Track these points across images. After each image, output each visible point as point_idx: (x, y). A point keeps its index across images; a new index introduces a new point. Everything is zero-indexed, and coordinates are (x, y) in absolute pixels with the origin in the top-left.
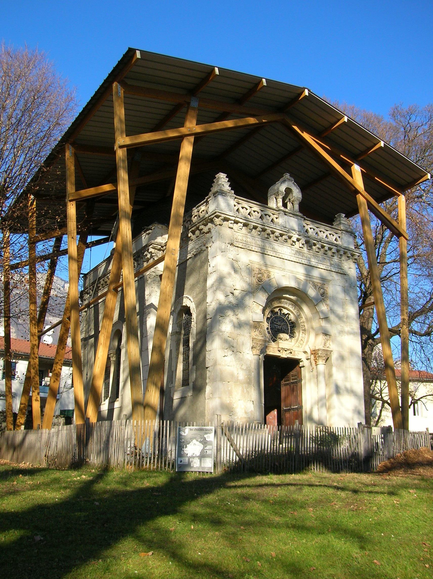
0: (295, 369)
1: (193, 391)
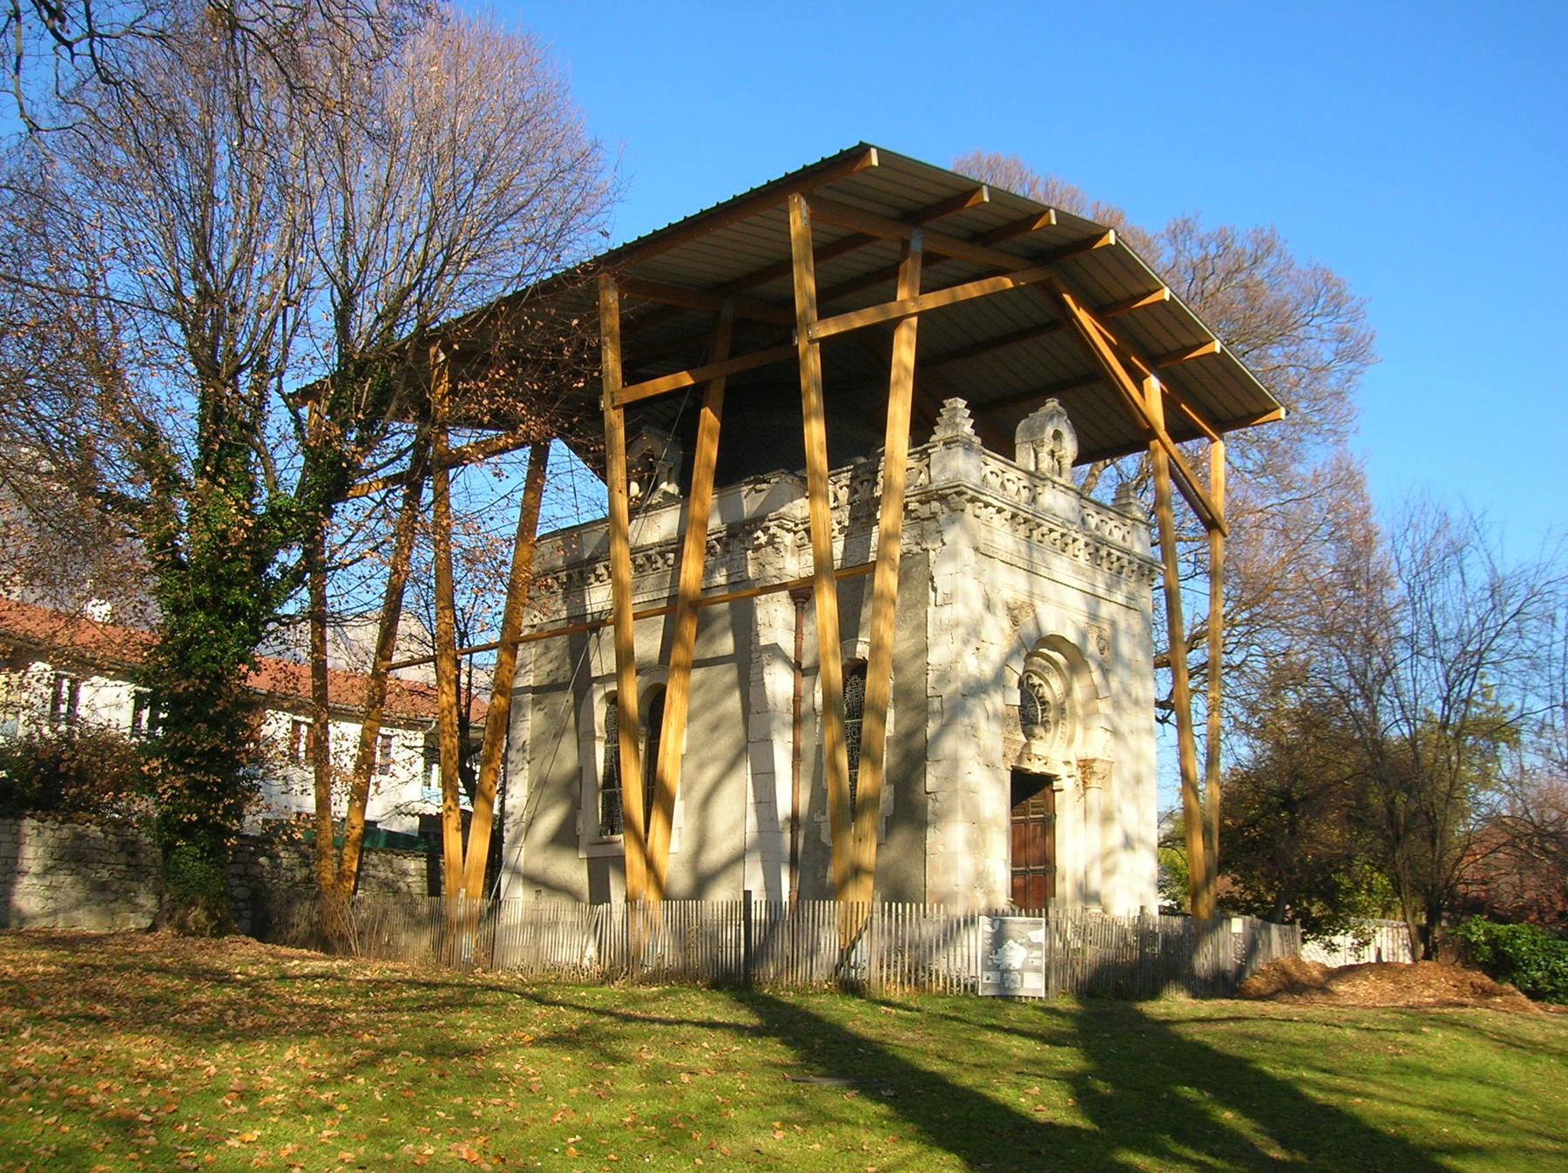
1: (1273, 922)
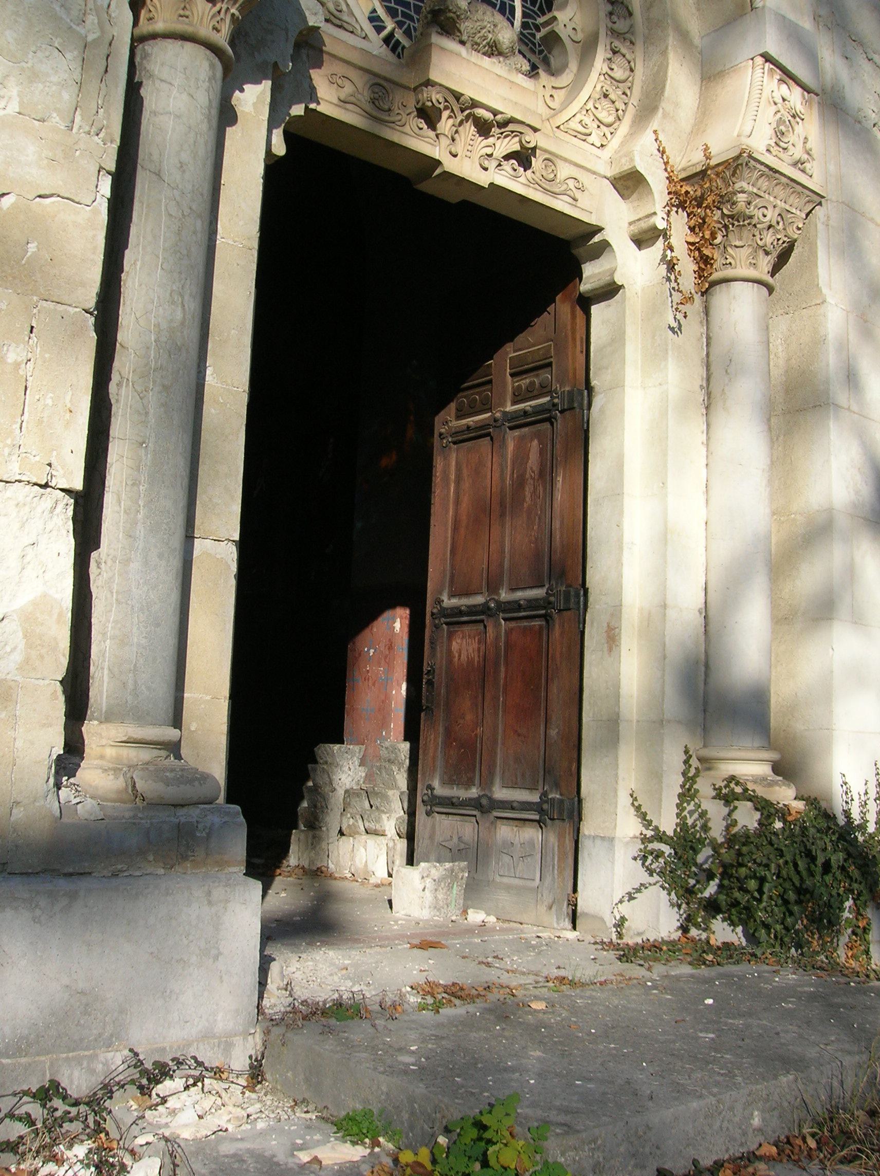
0: (545, 319)
